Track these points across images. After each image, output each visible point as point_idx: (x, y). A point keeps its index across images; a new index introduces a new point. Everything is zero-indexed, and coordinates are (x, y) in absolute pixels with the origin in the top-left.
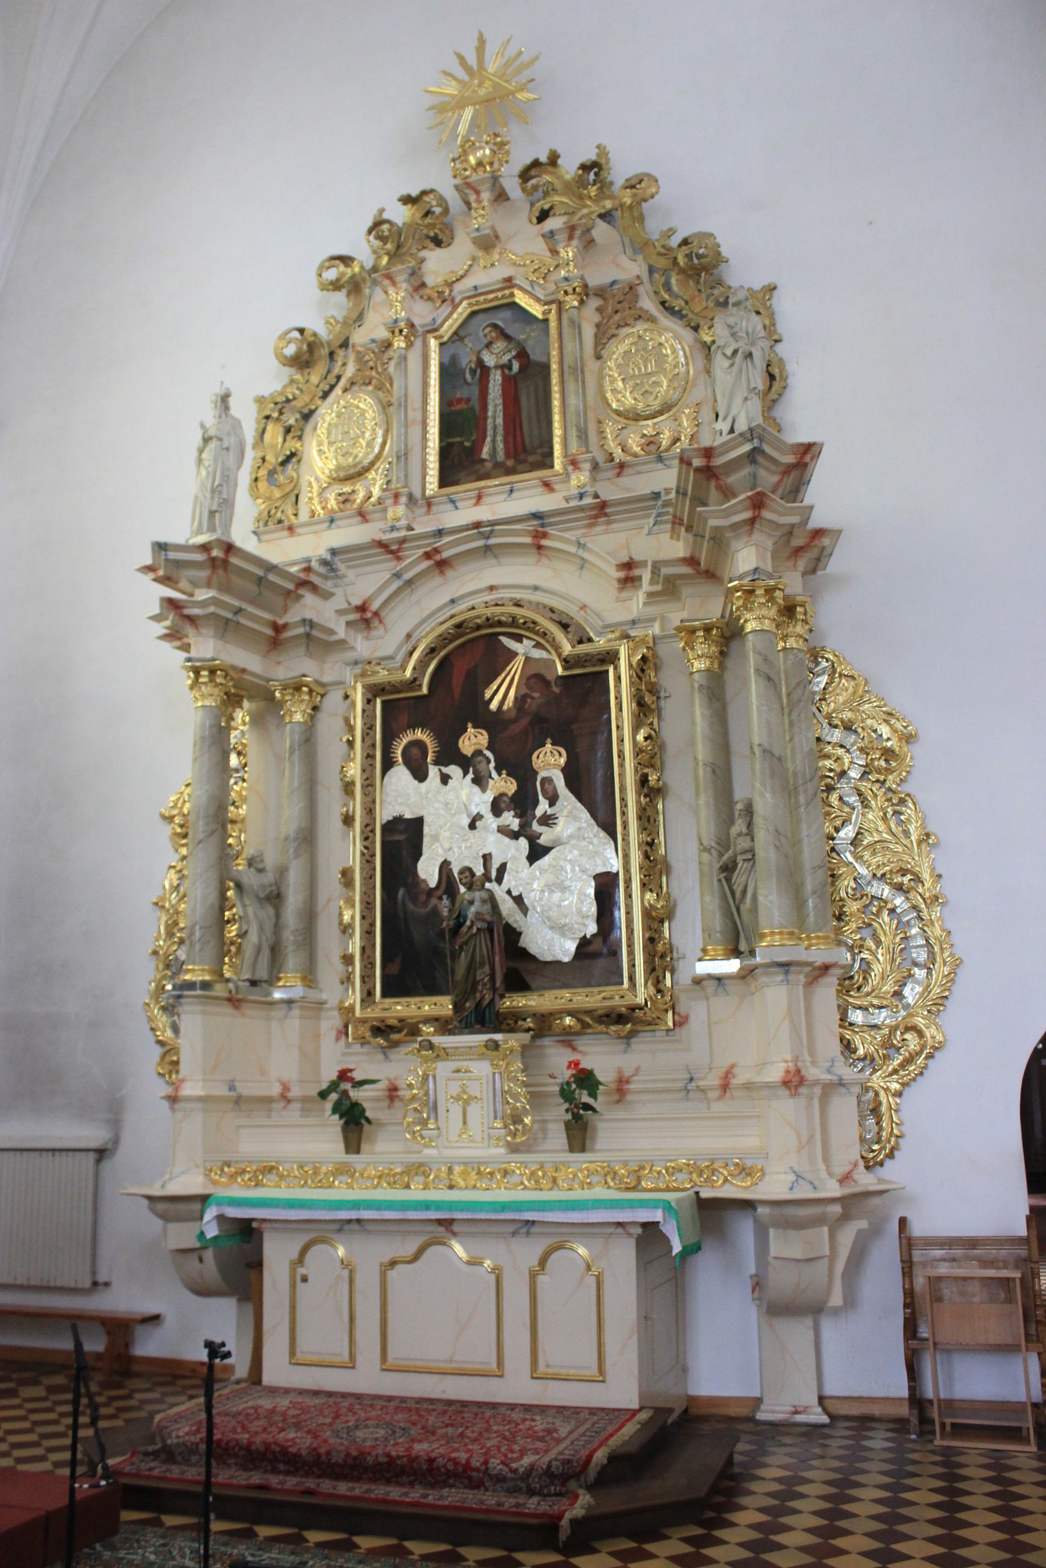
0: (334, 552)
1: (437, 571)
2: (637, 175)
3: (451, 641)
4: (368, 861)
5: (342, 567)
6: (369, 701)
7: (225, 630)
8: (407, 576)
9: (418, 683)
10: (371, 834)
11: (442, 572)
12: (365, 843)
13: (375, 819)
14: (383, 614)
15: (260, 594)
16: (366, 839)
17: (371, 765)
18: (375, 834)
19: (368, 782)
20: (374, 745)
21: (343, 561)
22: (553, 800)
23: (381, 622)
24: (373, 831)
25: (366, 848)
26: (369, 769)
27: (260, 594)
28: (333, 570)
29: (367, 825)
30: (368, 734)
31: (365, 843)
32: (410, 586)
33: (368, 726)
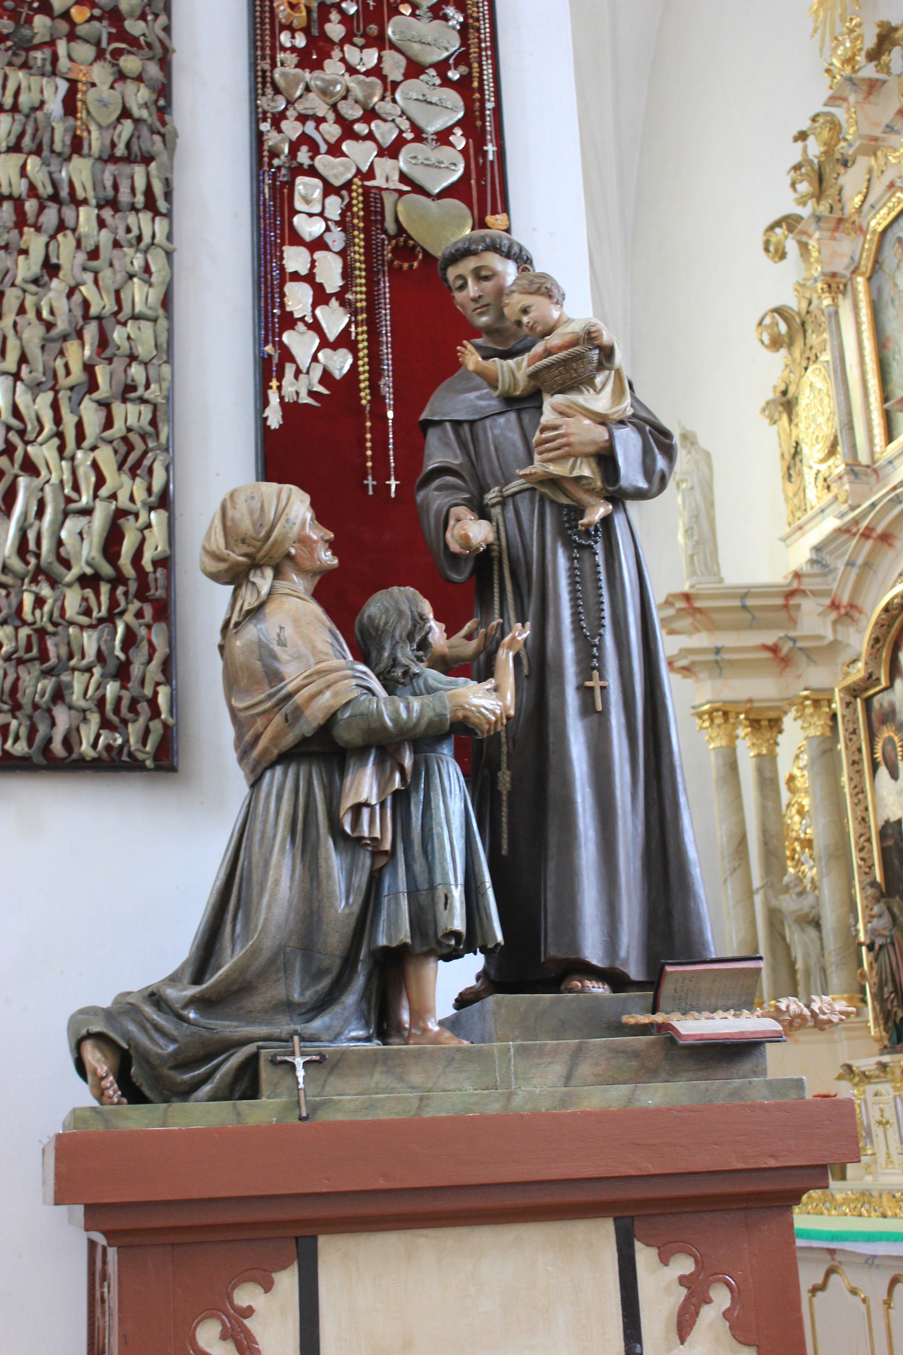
0: (817, 549)
1: (886, 546)
2: (176, 135)
3: (890, 626)
4: (866, 873)
5: (828, 559)
6: (848, 705)
7: (721, 669)
8: (860, 561)
9: (874, 678)
10: (866, 844)
11: (890, 545)
12: (862, 855)
13: (869, 827)
14: (859, 602)
15: (754, 618)
16: (861, 850)
17: (858, 772)
18: (871, 843)
19: (857, 790)
20: (860, 750)
21: (831, 553)
22: (798, 863)
23: (860, 612)
24: (869, 840)
25: (862, 859)
26: (856, 777)
27: (754, 618)
28: (825, 566)
29: (861, 835)
30: (851, 740)
31: (862, 855)
32: (870, 568)
33: (851, 729)
